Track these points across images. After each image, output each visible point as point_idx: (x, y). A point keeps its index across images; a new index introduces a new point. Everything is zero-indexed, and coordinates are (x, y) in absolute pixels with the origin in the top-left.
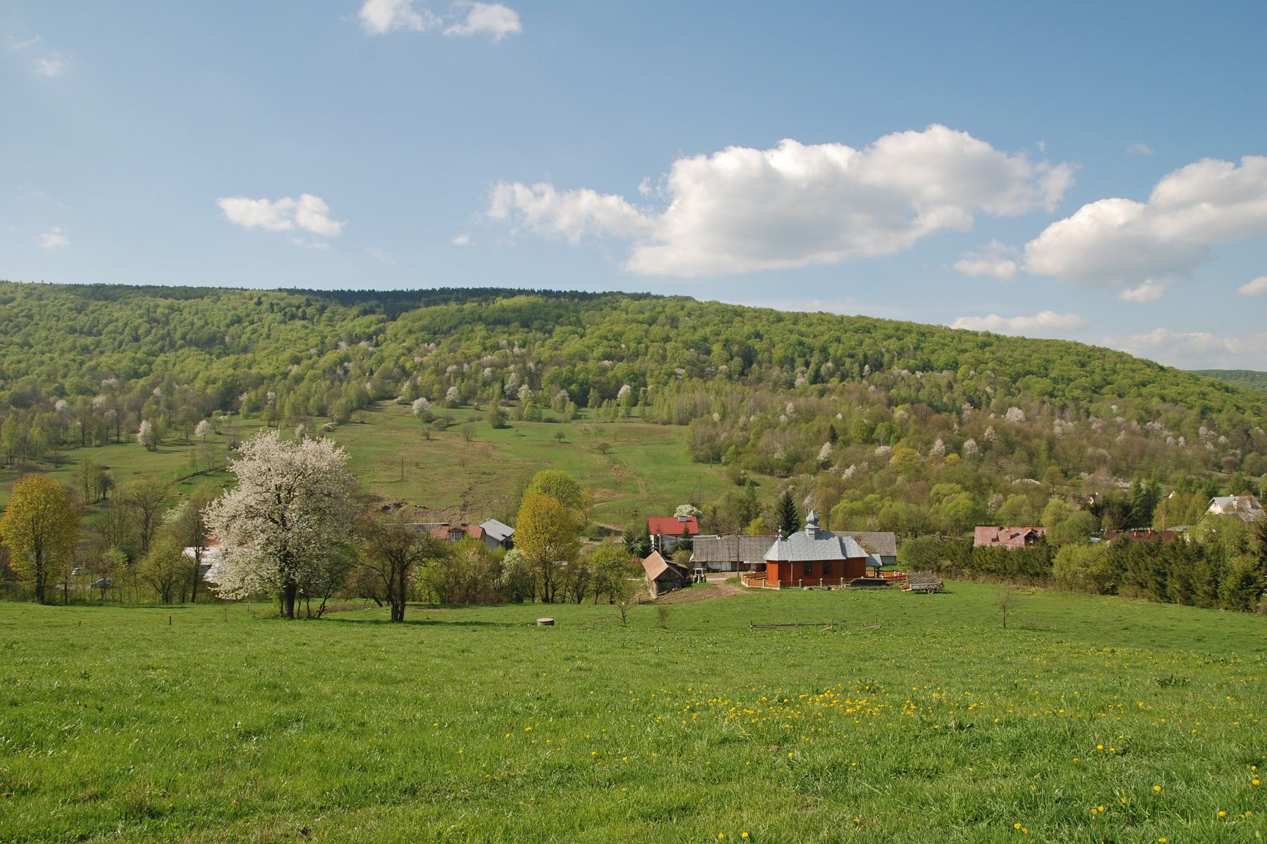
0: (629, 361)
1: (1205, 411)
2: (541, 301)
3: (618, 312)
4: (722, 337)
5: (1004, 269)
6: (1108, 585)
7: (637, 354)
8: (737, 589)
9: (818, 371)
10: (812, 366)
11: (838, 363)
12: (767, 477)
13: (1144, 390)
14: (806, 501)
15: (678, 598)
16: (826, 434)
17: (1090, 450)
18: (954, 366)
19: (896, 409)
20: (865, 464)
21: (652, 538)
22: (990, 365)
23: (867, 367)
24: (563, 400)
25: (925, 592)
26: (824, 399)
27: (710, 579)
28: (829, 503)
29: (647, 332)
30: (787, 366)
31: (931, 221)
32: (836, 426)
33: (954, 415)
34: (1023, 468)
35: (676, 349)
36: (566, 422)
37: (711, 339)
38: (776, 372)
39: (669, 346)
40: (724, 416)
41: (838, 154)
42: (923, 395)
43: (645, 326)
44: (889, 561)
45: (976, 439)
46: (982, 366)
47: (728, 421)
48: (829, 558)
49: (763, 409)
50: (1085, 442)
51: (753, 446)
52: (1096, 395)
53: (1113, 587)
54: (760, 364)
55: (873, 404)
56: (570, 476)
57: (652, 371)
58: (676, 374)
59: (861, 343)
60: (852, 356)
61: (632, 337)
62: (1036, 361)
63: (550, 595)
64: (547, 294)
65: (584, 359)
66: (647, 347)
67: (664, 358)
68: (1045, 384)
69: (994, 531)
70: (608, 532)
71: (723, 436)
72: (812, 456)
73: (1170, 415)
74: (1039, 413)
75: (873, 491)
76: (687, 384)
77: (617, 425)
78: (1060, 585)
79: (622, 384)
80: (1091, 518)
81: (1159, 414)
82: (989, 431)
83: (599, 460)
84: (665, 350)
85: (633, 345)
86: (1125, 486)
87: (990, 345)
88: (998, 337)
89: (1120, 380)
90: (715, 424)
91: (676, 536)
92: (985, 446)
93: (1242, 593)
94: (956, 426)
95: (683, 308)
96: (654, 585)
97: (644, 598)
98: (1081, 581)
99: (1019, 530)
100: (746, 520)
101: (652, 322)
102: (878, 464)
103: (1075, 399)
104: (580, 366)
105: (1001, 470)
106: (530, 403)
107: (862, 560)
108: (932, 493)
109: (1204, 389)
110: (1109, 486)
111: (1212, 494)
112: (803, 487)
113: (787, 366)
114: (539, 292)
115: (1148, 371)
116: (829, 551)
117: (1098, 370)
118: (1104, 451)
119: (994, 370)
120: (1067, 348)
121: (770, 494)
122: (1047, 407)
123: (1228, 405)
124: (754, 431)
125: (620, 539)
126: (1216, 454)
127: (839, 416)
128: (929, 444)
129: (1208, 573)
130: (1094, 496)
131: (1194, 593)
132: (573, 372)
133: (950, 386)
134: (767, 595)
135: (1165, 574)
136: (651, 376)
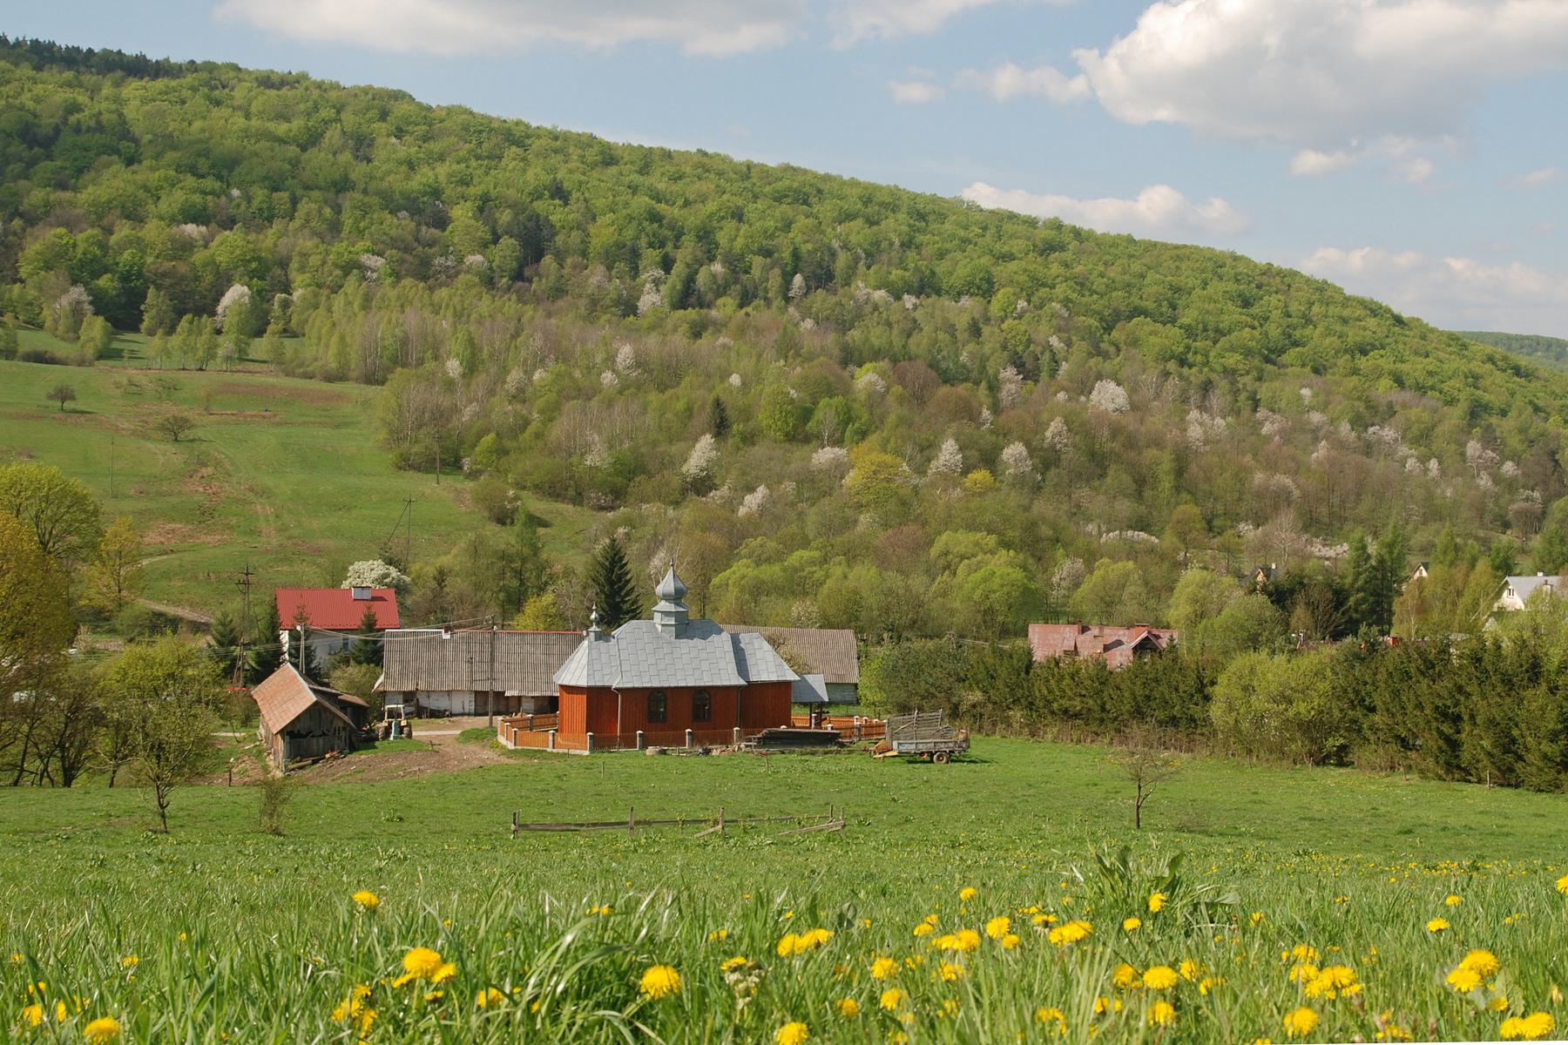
0: (248, 228)
1: (1477, 411)
3: (225, 112)
6: (1332, 743)
8: (487, 755)
9: (690, 281)
10: (679, 269)
11: (737, 266)
13: (1363, 363)
15: (343, 776)
16: (705, 416)
17: (1259, 477)
18: (986, 288)
19: (858, 372)
20: (789, 486)
21: (285, 637)
22: (1060, 290)
23: (798, 279)
24: (77, 313)
25: (929, 757)
26: (705, 342)
27: (423, 731)
28: (708, 565)
30: (621, 266)
33: (983, 390)
34: (1125, 507)
36: (81, 363)
38: (596, 276)
40: (471, 368)
42: (919, 344)
44: (844, 694)
45: (1027, 444)
46: (1043, 292)
47: (481, 379)
48: (706, 681)
49: (564, 356)
51: (538, 436)
52: (1270, 367)
53: (1343, 748)
54: (560, 257)
55: (810, 358)
56: (78, 484)
57: (305, 256)
59: (787, 226)
60: (767, 253)
62: (1153, 287)
65: (135, 216)
68: (1170, 337)
70: (174, 623)
73: (1414, 413)
74: (1157, 396)
75: (805, 543)
77: (212, 377)
78: (1225, 744)
79: (229, 283)
81: (1391, 412)
83: (164, 455)
86: (1332, 555)
87: (1062, 248)
88: (1077, 233)
89: (1318, 339)
90: (450, 385)
92: (1047, 459)
94: (986, 413)
95: (384, 115)
96: (280, 744)
98: (1273, 736)
99: (1122, 634)
100: (514, 602)
101: (311, 140)
102: (816, 485)
103: (1229, 373)
104: (123, 231)
105: (1078, 513)
107: (786, 685)
108: (934, 551)
109: (1476, 366)
110: (1295, 553)
111: (1505, 568)
112: (648, 531)
113: (621, 266)
114: (18, 44)
115: (1372, 322)
116: (707, 664)
117: (1276, 315)
119: (1066, 302)
120: (1217, 265)
121: (573, 543)
122: (1173, 383)
123: (1519, 402)
124: (540, 403)
125: (204, 641)
126: (1497, 497)
127: (735, 379)
128: (928, 449)
131: (1520, 758)
132: (103, 246)
133: (975, 331)
134: (560, 765)
135: (1457, 719)
136: (302, 269)
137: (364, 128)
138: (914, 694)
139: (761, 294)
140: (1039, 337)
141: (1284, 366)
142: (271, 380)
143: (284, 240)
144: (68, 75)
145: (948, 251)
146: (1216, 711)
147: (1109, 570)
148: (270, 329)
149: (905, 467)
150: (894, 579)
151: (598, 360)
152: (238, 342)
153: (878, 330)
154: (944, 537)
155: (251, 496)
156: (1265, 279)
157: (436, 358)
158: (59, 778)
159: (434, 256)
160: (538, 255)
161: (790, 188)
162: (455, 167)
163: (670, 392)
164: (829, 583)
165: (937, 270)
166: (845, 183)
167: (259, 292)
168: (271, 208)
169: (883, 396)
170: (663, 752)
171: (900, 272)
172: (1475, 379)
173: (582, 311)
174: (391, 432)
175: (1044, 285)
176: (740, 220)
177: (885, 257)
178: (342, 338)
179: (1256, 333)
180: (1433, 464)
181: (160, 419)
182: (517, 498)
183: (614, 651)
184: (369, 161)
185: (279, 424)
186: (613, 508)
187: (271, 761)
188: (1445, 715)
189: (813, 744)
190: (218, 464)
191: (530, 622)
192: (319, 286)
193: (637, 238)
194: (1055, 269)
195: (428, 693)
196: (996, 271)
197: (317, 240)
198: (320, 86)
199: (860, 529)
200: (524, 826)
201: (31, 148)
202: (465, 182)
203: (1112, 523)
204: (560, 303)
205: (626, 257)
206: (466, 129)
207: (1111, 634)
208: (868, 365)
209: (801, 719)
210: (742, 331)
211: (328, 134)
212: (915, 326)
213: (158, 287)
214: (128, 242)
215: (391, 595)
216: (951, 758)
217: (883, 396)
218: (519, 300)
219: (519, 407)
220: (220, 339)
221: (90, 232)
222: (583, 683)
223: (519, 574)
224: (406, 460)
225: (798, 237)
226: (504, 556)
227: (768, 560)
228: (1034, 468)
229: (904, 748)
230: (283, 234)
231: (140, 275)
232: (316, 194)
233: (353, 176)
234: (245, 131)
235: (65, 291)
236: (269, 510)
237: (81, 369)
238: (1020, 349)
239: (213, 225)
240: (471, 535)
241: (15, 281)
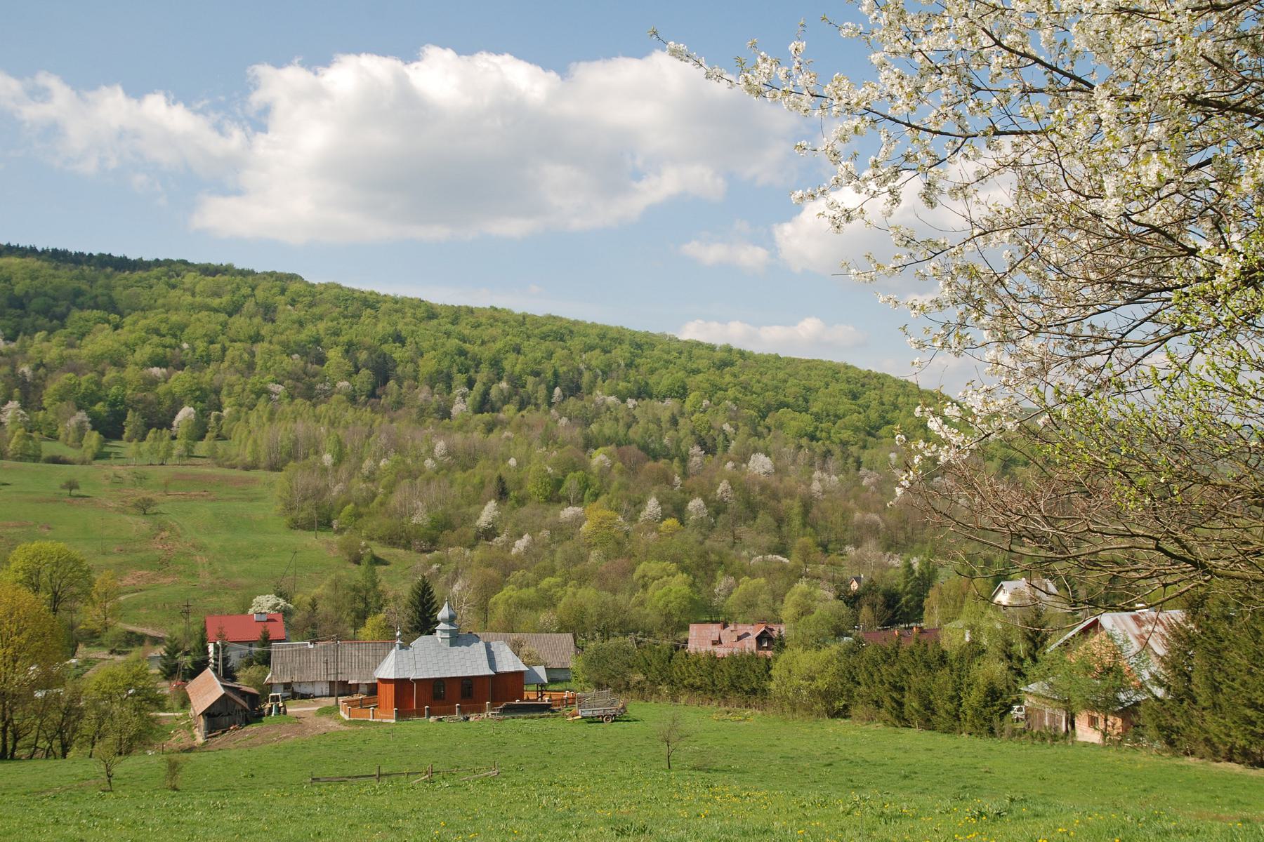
0: (193, 369)
1: (1007, 464)
2: (46, 268)
3: (178, 292)
4: (343, 339)
5: (751, 256)
6: (839, 704)
7: (206, 360)
8: (332, 724)
9: (486, 394)
10: (478, 387)
11: (517, 383)
12: (400, 552)
14: (456, 588)
15: (241, 742)
16: (492, 487)
17: (858, 516)
18: (681, 393)
20: (545, 533)
22: (731, 393)
23: (557, 391)
24: (81, 429)
26: (493, 437)
27: (293, 709)
28: (488, 589)
29: (224, 325)
30: (440, 386)
31: (665, 185)
32: (508, 477)
34: (767, 539)
35: (271, 354)
36: (83, 463)
37: (326, 341)
38: (423, 393)
39: (259, 348)
40: (339, 458)
41: (521, 78)
42: (636, 433)
43: (222, 317)
44: (557, 676)
45: (705, 499)
49: (400, 450)
50: (851, 504)
51: (382, 504)
52: (871, 439)
53: (845, 707)
54: (400, 382)
55: (562, 446)
57: (231, 386)
58: (268, 392)
59: (550, 355)
60: (536, 374)
61: (201, 331)
63: (10, 747)
64: (58, 256)
65: (119, 363)
66: (224, 350)
67: (251, 366)
68: (803, 421)
69: (714, 630)
70: (139, 639)
71: (336, 490)
72: (468, 520)
74: (794, 461)
75: (552, 572)
76: (286, 407)
79: (181, 405)
80: (845, 610)
82: (723, 486)
83: (137, 524)
84: (252, 354)
85: (201, 345)
87: (732, 364)
88: (742, 354)
90: (325, 470)
91: (250, 643)
92: (717, 508)
93: (986, 712)
94: (677, 479)
96: (202, 722)
97: (186, 743)
100: (361, 618)
101: (234, 309)
102: (563, 532)
103: (844, 444)
104: (111, 373)
106: (20, 432)
107: (519, 674)
108: (636, 576)
111: (1000, 578)
112: (453, 566)
113: (440, 386)
114: (44, 252)
116: (470, 662)
117: (874, 404)
118: (875, 517)
119: (735, 400)
120: (835, 372)
124: (384, 481)
125: (160, 651)
127: (513, 462)
128: (639, 504)
129: (950, 686)
130: (858, 580)
131: (934, 713)
133: (674, 422)
135: (902, 689)
136: (229, 395)
137: (270, 300)
138: (609, 677)
139: (533, 401)
140: (716, 425)
141: (881, 438)
142: (208, 470)
143: (218, 376)
145: (656, 369)
148: (208, 435)
149: (620, 519)
151: (423, 451)
152: (187, 445)
153: (610, 424)
154: (642, 566)
155: (193, 551)
156: (866, 380)
157: (317, 453)
158: (59, 751)
159: (316, 383)
160: (386, 380)
161: (551, 331)
162: (330, 324)
163: (470, 471)
165: (650, 381)
166: (587, 326)
167: (201, 411)
168: (208, 355)
169: (610, 470)
170: (440, 720)
171: (625, 384)
173: (415, 416)
174: (285, 505)
175: (720, 389)
176: (519, 353)
177: (614, 374)
178: (255, 441)
179: (861, 416)
181: (135, 500)
182: (367, 547)
183: (411, 656)
184: (273, 321)
185: (213, 500)
186: (430, 551)
187: (196, 732)
188: (895, 687)
189: (534, 711)
190: (172, 529)
191: (369, 632)
192: (241, 405)
193: (451, 367)
195: (300, 683)
196: (688, 381)
197: (239, 375)
199: (592, 560)
200: (318, 780)
201: (51, 321)
202: (337, 333)
204: (400, 412)
206: (337, 298)
207: (742, 629)
208: (600, 449)
209: (530, 694)
210: (519, 427)
211: (246, 305)
212: (635, 420)
213: (135, 410)
214: (116, 381)
215: (280, 617)
216: (615, 719)
217: (610, 470)
218: (372, 411)
219: (370, 485)
220: (175, 443)
221: (90, 375)
222: (392, 677)
223: (364, 600)
224: (296, 522)
226: (354, 589)
227: (528, 586)
228: (709, 515)
229: (585, 714)
230: (217, 372)
231: (122, 402)
232: (238, 345)
233: (263, 332)
234: (191, 304)
237: (85, 467)
238: (703, 433)
239: (171, 368)
240: (333, 576)
241: (40, 409)
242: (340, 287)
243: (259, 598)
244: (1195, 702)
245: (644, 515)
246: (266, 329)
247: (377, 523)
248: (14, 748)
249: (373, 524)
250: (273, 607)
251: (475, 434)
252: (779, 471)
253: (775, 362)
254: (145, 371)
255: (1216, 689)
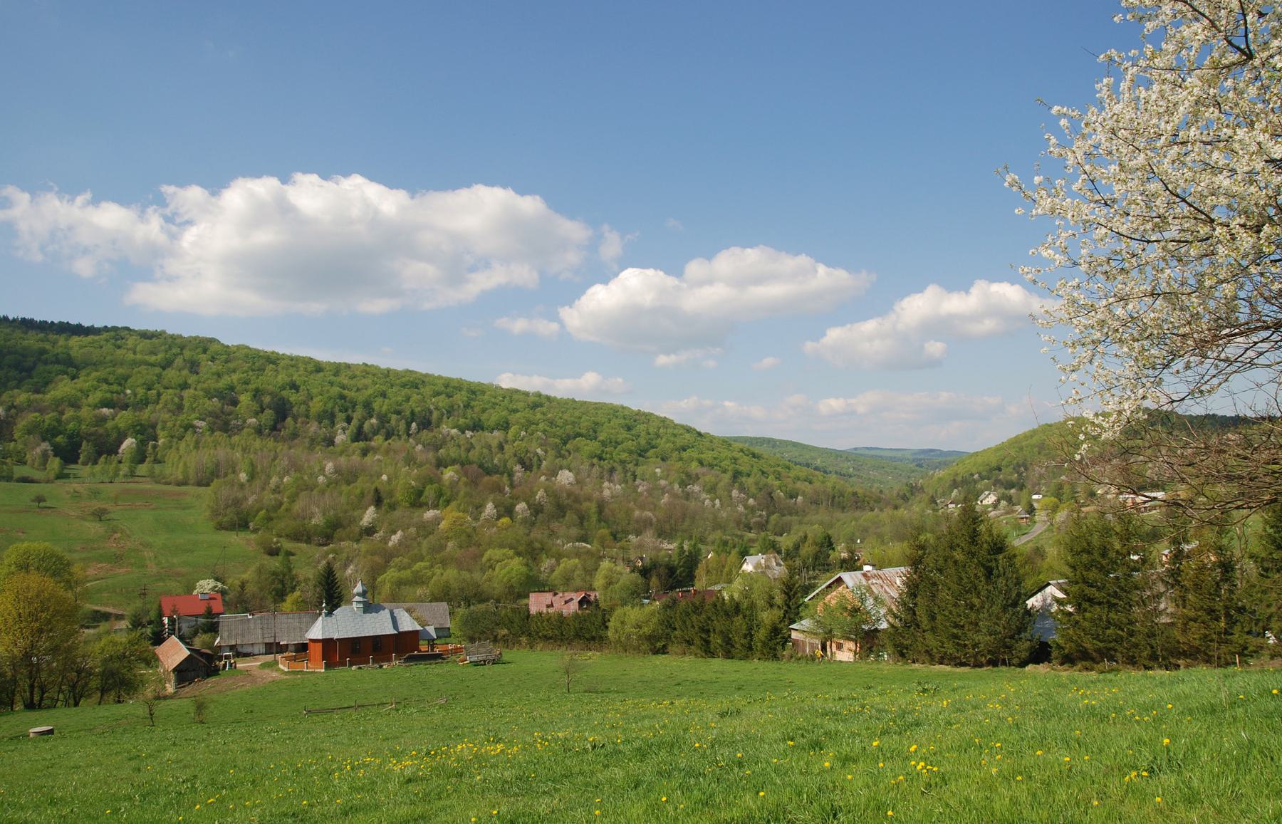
0: (135, 410)
1: (736, 475)
6: (659, 645)
7: (145, 403)
8: (274, 674)
10: (355, 422)
11: (383, 419)
13: (685, 455)
14: (349, 571)
15: (206, 687)
16: (370, 497)
17: (637, 513)
18: (505, 426)
19: (445, 471)
20: (413, 530)
21: (166, 620)
22: (541, 426)
23: (414, 425)
24: (45, 456)
25: (484, 663)
26: (368, 459)
27: (242, 664)
28: (373, 574)
29: (159, 376)
33: (505, 478)
34: (574, 531)
35: (195, 398)
36: (48, 482)
37: (238, 388)
38: (313, 427)
39: (187, 394)
40: (252, 476)
43: (158, 370)
44: (444, 633)
45: (527, 503)
47: (258, 483)
48: (379, 633)
49: (299, 469)
51: (287, 510)
54: (295, 419)
55: (420, 465)
56: (58, 549)
57: (165, 422)
58: (194, 427)
59: (408, 399)
60: (398, 413)
61: (141, 381)
62: (585, 423)
64: (27, 324)
65: (75, 405)
67: (180, 408)
68: (594, 446)
69: (547, 598)
70: (106, 617)
71: (251, 500)
72: (353, 521)
73: (707, 478)
75: (422, 559)
76: (208, 438)
80: (640, 580)
84: (181, 398)
85: (141, 391)
87: (541, 405)
88: (548, 398)
90: (242, 486)
91: (197, 616)
92: (537, 510)
94: (507, 489)
98: (635, 643)
99: (573, 595)
100: (280, 595)
101: (167, 365)
102: (427, 529)
103: (622, 462)
105: (553, 534)
108: (484, 559)
111: (744, 553)
112: (345, 555)
113: (326, 422)
114: (14, 320)
115: (687, 436)
116: (379, 625)
117: (643, 434)
118: (649, 514)
119: (544, 431)
120: (615, 411)
121: (308, 564)
122: (596, 469)
123: (755, 470)
124: (288, 493)
126: (746, 515)
127: (384, 477)
128: (480, 507)
130: (642, 559)
132: (59, 421)
133: (501, 447)
135: (708, 631)
136: (163, 429)
138: (477, 631)
140: (532, 450)
144: (41, 335)
146: (610, 633)
147: (567, 564)
150: (466, 575)
157: (234, 472)
164: (435, 578)
172: (735, 460)
178: (185, 464)
180: (717, 501)
190: (122, 531)
194: (539, 416)
196: (510, 418)
198: (172, 337)
202: (247, 383)
203: (570, 539)
205: (328, 417)
210: (387, 452)
212: (470, 448)
214: (73, 418)
222: (320, 637)
223: (282, 582)
225: (414, 404)
226: (274, 574)
227: (405, 568)
235: (38, 445)
236: (151, 554)
240: (258, 564)
242: (248, 348)
243: (202, 582)
244: (918, 626)
245: (483, 516)
246: (192, 379)
247: (283, 524)
248: (42, 699)
249: (282, 525)
250: (213, 589)
251: (354, 457)
252: (578, 482)
253: (569, 405)
254: (97, 411)
255: (933, 618)
